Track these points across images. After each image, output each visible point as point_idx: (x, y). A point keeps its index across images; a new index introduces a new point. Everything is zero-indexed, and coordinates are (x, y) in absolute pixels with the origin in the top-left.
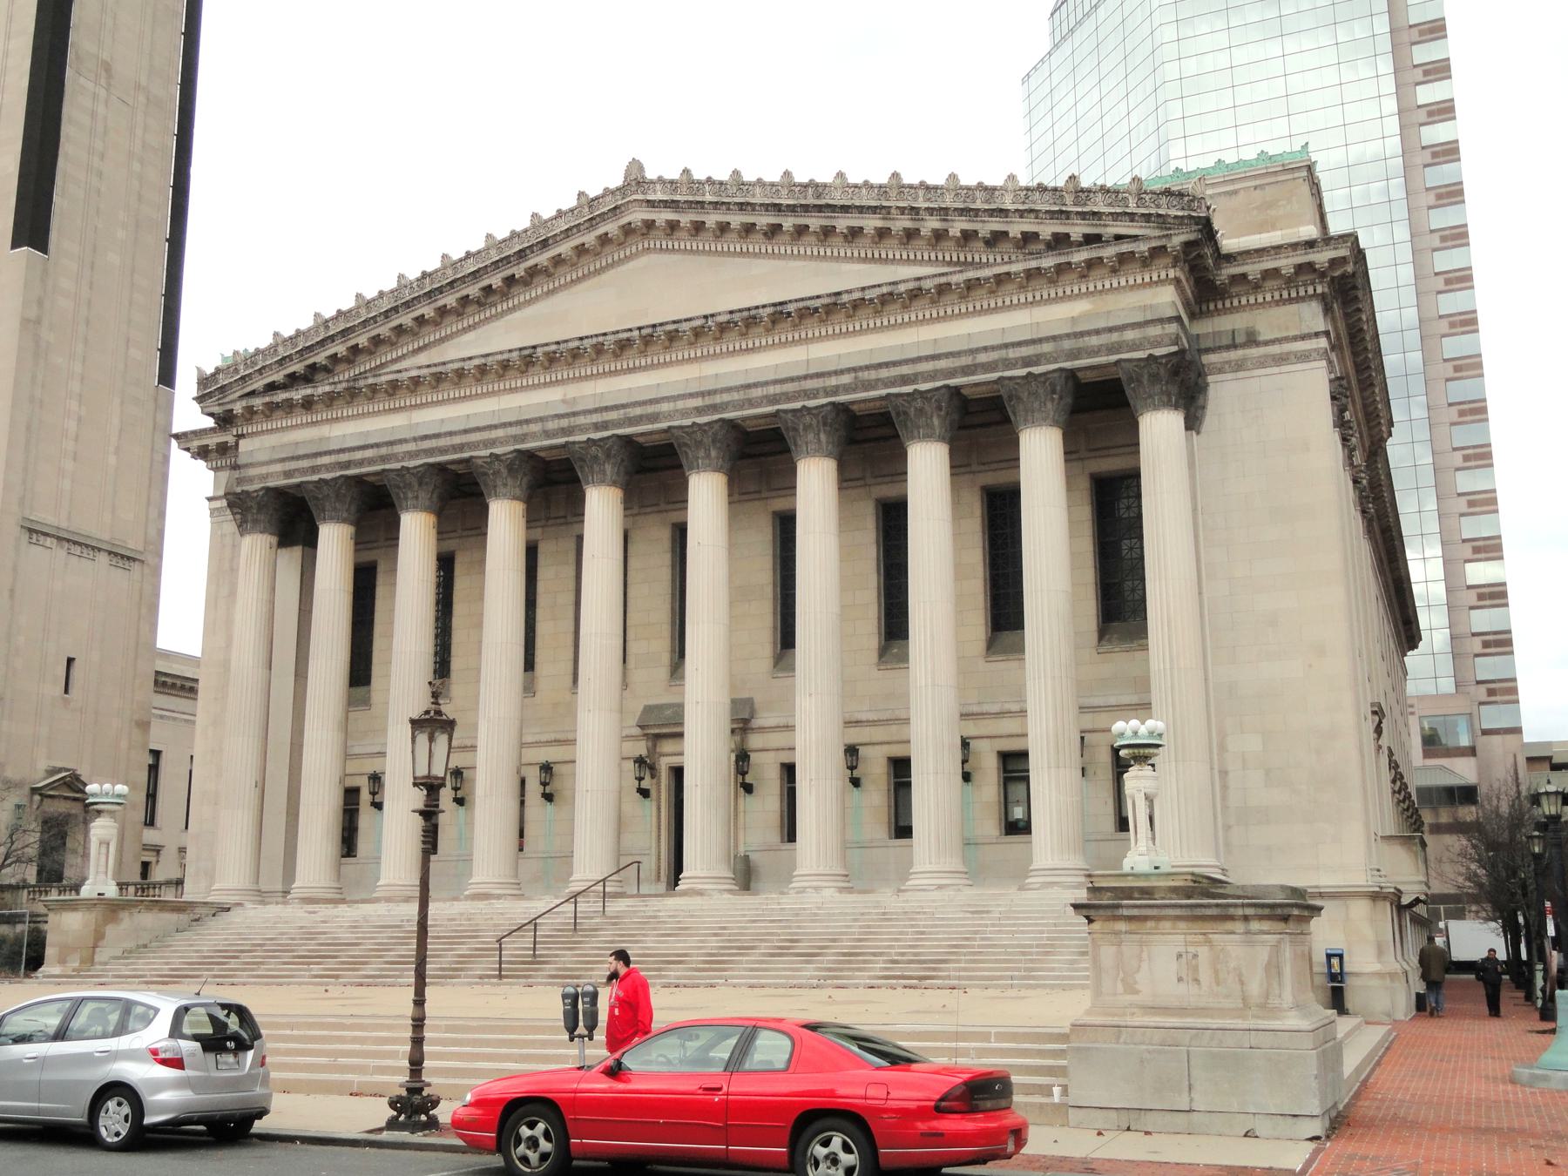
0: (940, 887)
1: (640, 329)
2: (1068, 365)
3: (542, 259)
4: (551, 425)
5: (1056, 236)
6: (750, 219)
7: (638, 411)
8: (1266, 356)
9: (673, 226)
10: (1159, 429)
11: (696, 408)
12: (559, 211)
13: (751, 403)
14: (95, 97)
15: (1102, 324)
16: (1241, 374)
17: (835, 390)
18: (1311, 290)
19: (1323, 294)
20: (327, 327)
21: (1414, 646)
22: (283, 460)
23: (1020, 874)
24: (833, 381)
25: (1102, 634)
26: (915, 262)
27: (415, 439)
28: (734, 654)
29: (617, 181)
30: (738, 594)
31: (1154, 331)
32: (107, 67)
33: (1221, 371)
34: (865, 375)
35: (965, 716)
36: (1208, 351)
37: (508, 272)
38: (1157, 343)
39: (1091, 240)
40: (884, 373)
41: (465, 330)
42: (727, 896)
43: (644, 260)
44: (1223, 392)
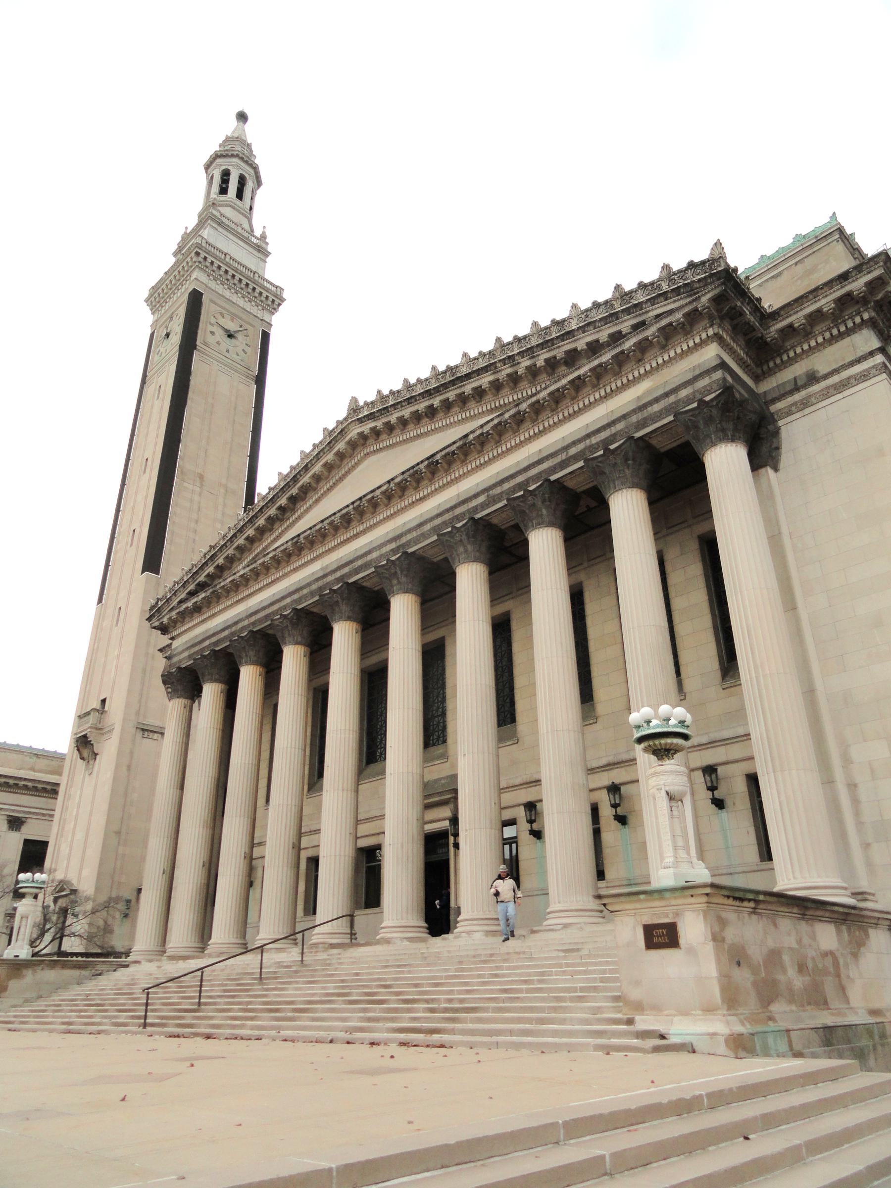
0: (566, 926)
8: (828, 388)
14: (193, 491)
18: (858, 320)
19: (871, 319)
29: (342, 414)
32: (201, 477)
33: (789, 413)
36: (774, 401)
42: (406, 943)
43: (366, 463)
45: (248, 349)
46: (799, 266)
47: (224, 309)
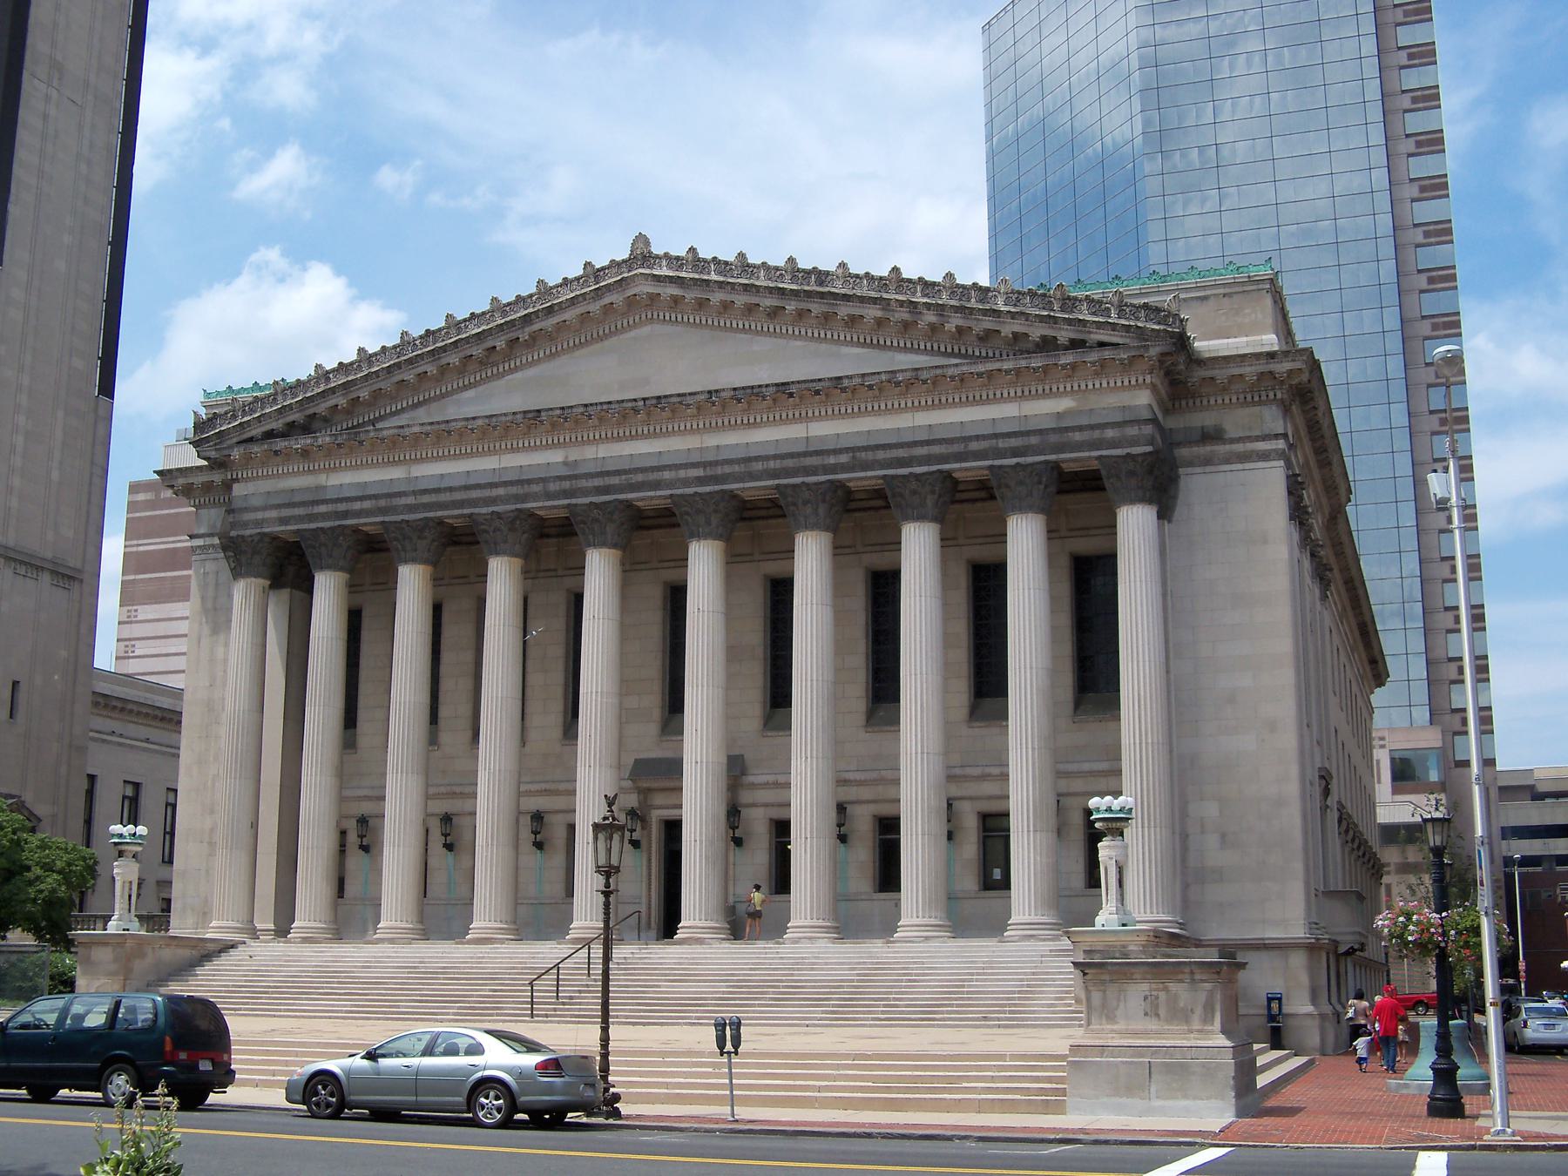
1: (644, 399)
2: (1053, 457)
3: (549, 323)
4: (553, 487)
5: (1044, 338)
6: (754, 300)
7: (640, 477)
9: (676, 300)
10: (1135, 525)
11: (698, 478)
12: (565, 279)
13: (752, 476)
14: (48, 98)
15: (1084, 421)
16: (1208, 469)
17: (834, 469)
20: (328, 380)
21: (1381, 684)
22: (279, 506)
23: (996, 926)
24: (832, 460)
25: (1078, 704)
26: (912, 350)
27: (414, 493)
28: (730, 714)
30: (733, 653)
31: (1132, 431)
33: (1191, 464)
35: (951, 778)
36: (1179, 444)
37: (513, 335)
38: (1134, 442)
39: (1076, 344)
40: (881, 455)
41: (466, 388)
44: (1196, 485)
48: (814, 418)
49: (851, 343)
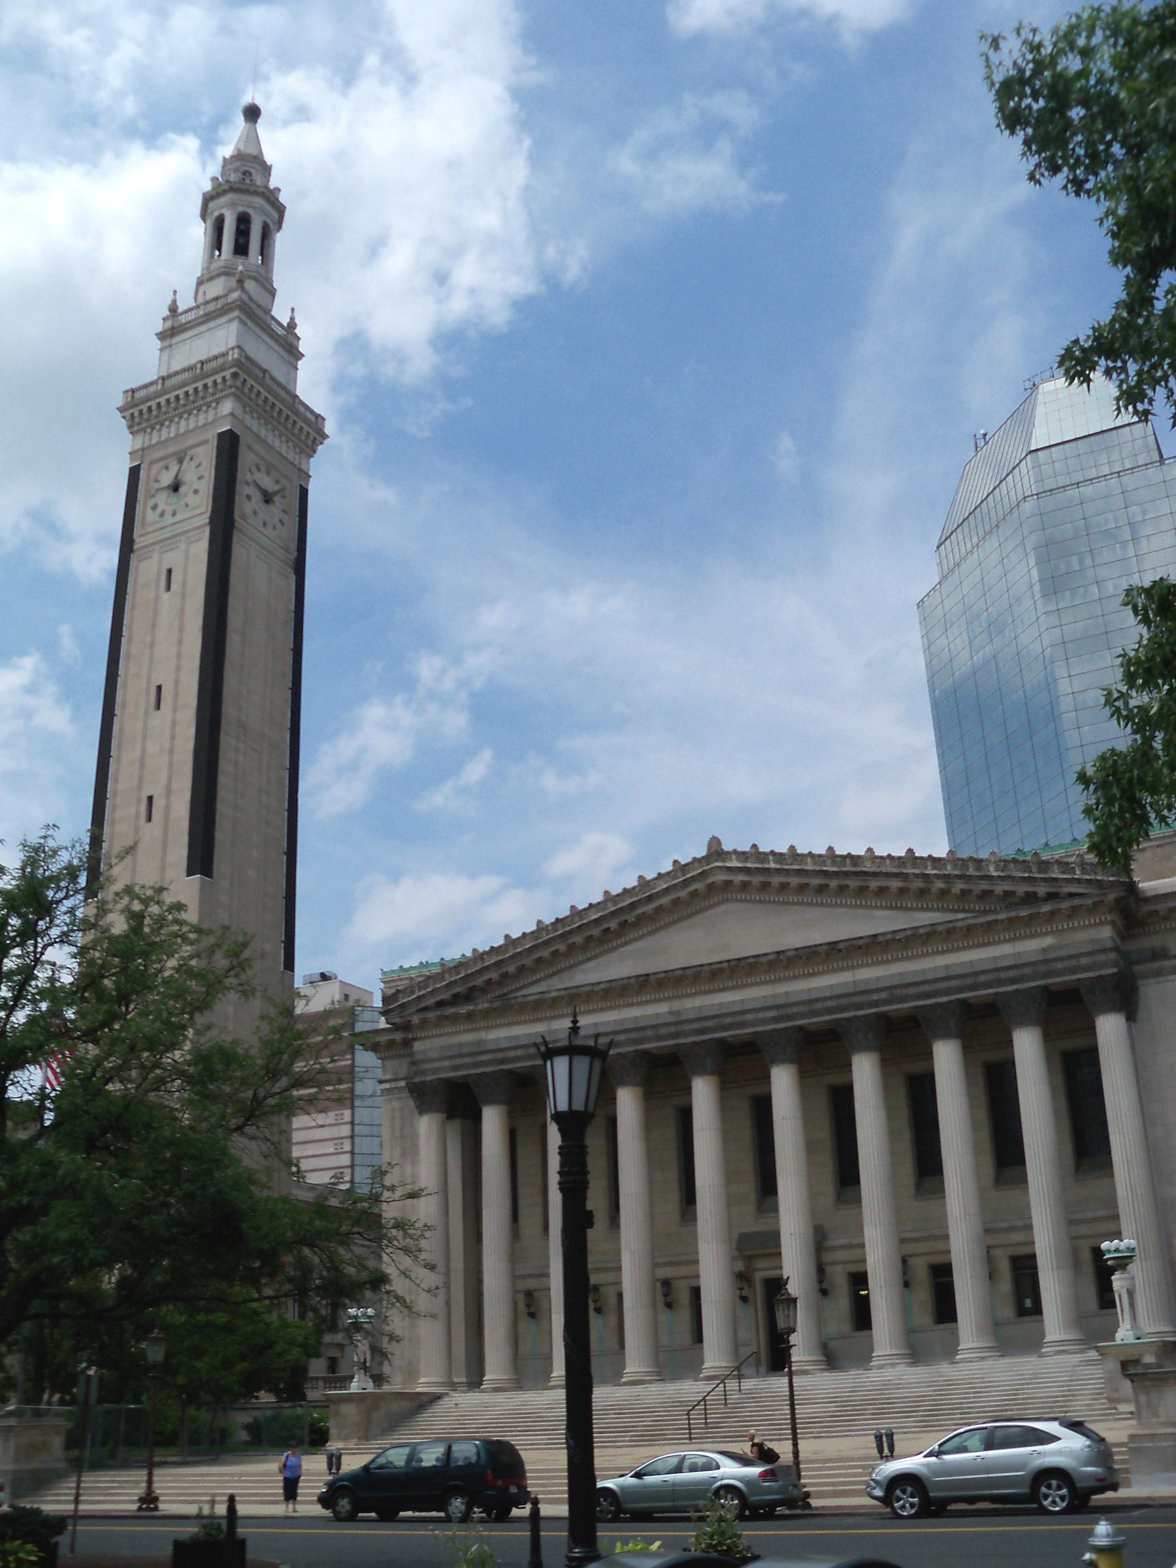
10: (1110, 1029)
31: (1101, 958)
34: (898, 992)
43: (723, 907)
45: (286, 518)
46: (1159, 850)
47: (262, 458)
48: (859, 966)
49: (881, 908)
